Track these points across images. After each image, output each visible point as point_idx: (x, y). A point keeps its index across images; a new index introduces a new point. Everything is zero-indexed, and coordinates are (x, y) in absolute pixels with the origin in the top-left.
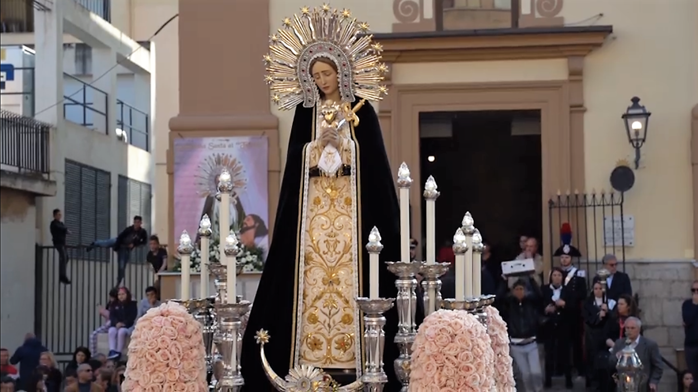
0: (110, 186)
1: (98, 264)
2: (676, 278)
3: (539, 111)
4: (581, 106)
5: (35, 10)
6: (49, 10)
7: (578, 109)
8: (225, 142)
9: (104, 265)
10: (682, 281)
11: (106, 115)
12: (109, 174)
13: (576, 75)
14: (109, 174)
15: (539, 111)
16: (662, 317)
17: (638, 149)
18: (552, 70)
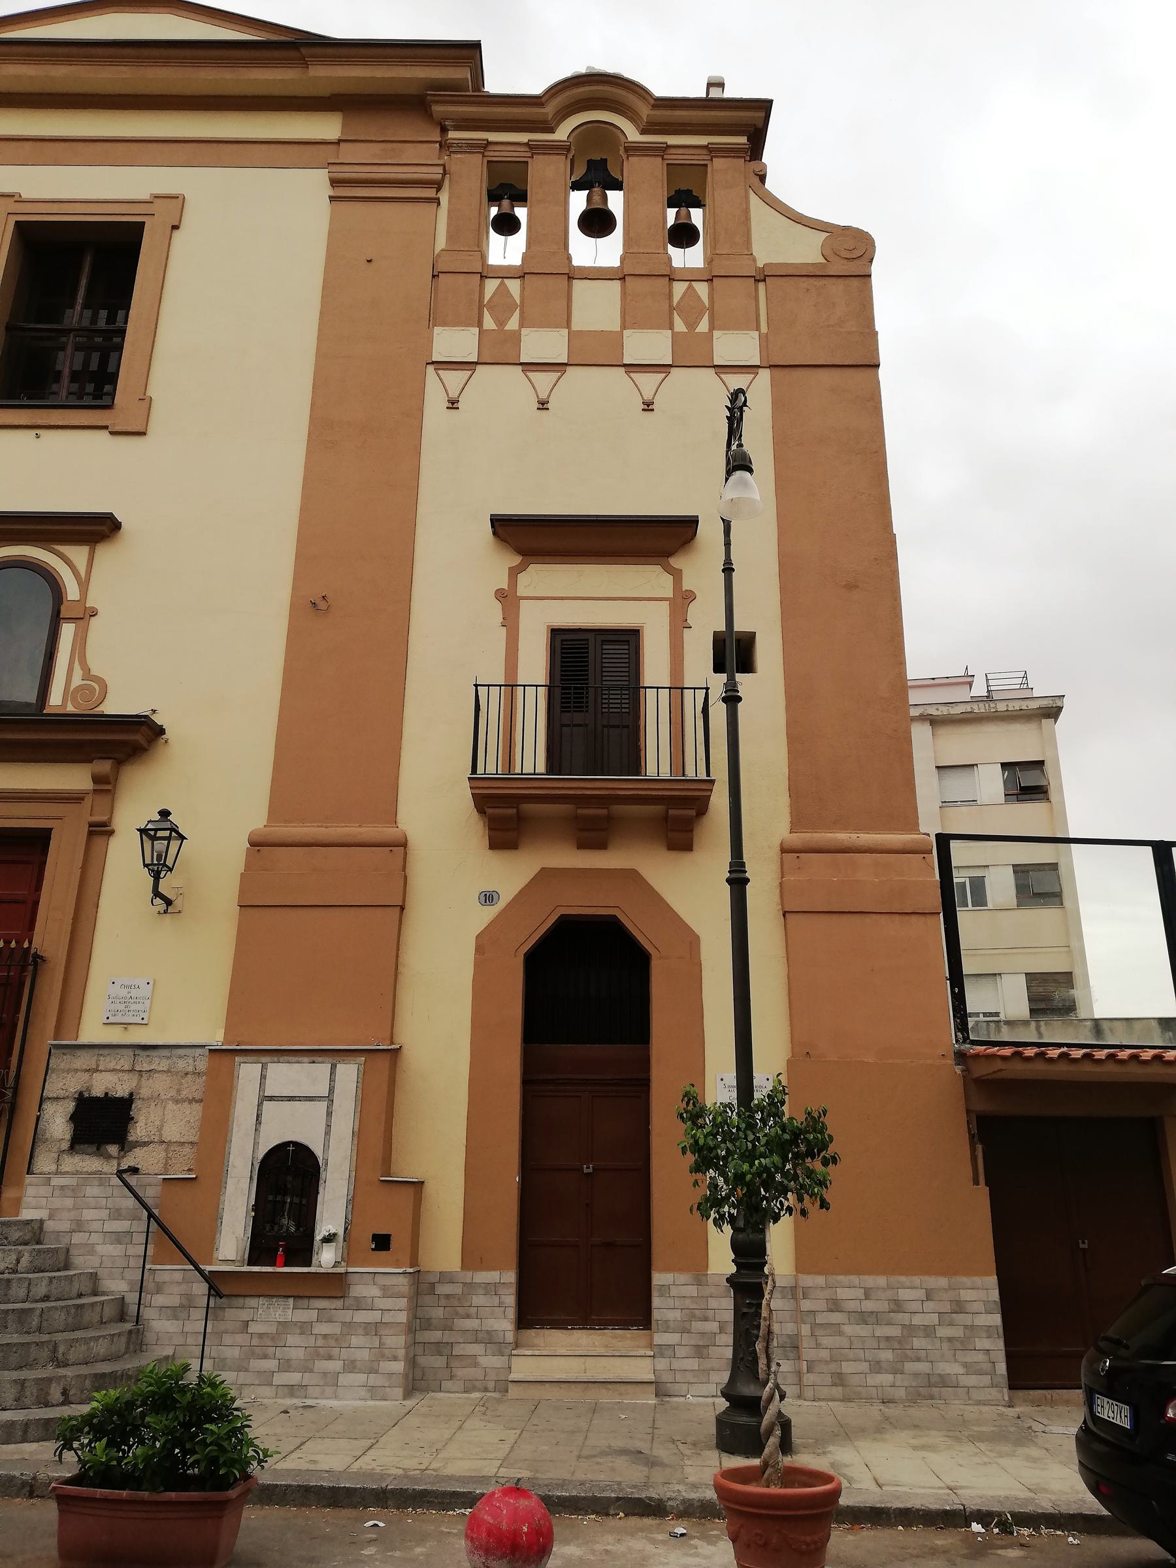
2: (190, 1069)
13: (106, 786)
18: (73, 778)
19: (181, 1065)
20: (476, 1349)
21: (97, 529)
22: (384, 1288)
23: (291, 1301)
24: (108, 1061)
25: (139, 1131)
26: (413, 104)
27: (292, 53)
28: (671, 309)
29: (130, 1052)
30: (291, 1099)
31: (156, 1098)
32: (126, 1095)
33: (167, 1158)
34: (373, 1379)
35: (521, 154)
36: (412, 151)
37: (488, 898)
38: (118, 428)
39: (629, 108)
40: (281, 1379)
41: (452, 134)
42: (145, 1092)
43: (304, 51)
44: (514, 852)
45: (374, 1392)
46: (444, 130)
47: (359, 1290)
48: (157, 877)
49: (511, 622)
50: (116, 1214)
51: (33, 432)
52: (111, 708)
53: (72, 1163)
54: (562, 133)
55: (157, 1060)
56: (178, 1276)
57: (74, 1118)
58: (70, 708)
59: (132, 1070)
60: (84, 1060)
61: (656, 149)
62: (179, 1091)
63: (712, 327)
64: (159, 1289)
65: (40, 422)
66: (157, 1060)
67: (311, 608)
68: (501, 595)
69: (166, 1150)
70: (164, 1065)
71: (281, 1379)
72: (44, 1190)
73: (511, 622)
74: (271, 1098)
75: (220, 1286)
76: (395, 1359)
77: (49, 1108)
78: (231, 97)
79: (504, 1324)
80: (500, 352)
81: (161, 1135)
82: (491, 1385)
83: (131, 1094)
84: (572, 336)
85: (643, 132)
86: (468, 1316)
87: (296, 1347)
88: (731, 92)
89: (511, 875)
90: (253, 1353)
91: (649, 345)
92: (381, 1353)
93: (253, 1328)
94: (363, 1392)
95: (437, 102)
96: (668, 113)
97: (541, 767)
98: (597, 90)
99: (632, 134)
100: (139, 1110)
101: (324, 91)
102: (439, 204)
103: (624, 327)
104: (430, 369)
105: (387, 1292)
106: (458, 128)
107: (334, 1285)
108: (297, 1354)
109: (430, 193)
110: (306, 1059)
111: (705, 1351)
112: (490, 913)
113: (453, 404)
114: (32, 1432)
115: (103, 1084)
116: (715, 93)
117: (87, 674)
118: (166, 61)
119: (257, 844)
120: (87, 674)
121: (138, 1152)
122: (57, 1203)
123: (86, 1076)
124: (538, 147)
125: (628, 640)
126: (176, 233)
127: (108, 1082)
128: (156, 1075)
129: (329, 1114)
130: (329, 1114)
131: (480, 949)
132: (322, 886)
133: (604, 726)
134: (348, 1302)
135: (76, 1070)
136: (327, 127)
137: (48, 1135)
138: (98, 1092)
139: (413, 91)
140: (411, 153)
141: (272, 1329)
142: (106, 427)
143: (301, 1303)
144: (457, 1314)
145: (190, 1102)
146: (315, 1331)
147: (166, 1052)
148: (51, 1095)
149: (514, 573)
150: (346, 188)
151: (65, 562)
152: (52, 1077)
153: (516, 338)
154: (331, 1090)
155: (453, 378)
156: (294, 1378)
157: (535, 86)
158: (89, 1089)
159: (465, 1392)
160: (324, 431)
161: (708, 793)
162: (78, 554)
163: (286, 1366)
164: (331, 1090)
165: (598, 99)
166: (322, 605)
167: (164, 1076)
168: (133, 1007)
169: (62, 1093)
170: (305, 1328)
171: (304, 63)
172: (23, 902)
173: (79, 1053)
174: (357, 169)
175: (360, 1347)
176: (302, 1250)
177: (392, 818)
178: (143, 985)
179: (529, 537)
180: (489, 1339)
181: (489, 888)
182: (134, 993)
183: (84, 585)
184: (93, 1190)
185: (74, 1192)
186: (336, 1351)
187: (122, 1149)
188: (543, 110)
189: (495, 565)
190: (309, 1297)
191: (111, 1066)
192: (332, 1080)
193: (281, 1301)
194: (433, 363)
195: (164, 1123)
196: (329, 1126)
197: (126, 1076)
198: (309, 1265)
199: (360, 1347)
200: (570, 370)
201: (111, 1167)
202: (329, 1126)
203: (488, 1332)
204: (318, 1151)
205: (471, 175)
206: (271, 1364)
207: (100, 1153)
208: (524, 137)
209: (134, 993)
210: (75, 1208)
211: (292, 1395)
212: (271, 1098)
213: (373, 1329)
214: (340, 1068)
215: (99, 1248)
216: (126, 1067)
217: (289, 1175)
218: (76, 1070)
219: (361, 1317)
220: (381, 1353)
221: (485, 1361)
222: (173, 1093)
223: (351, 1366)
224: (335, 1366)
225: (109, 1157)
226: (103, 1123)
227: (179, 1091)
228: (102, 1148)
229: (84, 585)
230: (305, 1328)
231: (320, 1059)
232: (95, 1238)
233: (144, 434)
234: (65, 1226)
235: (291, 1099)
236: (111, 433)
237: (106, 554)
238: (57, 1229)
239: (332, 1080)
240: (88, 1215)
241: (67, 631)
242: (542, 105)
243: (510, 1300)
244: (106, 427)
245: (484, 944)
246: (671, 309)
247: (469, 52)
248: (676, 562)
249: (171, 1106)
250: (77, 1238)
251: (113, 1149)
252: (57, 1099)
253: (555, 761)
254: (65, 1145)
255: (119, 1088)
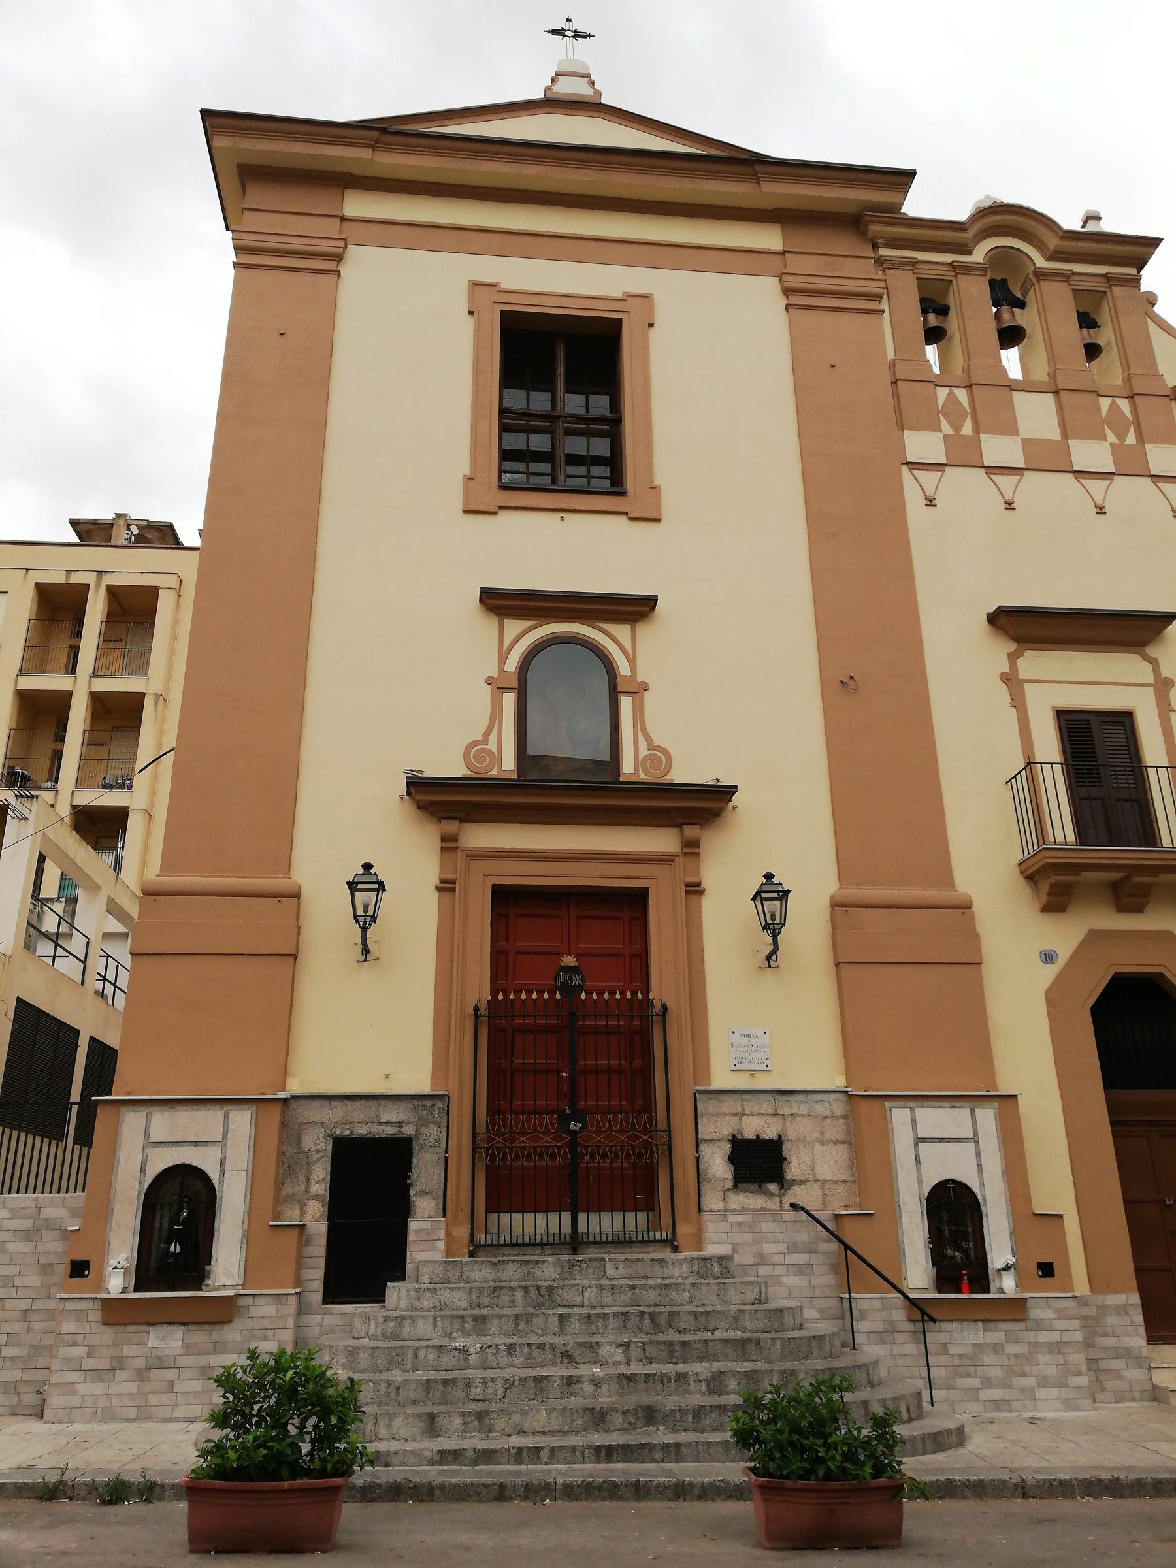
0: (77, 1046)
1: (46, 1141)
2: (828, 1113)
3: (645, 891)
4: (698, 885)
5: (9, 817)
6: (26, 819)
7: (695, 890)
8: (180, 1437)
9: (54, 1143)
10: (836, 1118)
11: (85, 963)
12: (78, 1032)
13: (692, 848)
14: (78, 1032)
15: (645, 891)
16: (813, 1168)
17: (775, 937)
18: (659, 841)
19: (819, 1109)
20: (1116, 1364)
21: (636, 609)
22: (1057, 1311)
23: (980, 1324)
24: (752, 1106)
25: (793, 1170)
26: (853, 222)
27: (748, 170)
28: (938, 412)
29: (769, 1097)
30: (941, 1140)
31: (801, 1140)
32: (775, 1137)
33: (824, 1195)
34: (1065, 1393)
35: (947, 274)
36: (848, 264)
37: (1048, 957)
38: (636, 515)
39: (1036, 238)
40: (986, 1394)
41: (883, 252)
42: (791, 1134)
43: (758, 168)
44: (1139, 915)
45: (1068, 1404)
46: (875, 247)
47: (1037, 1312)
48: (364, 929)
49: (1018, 702)
50: (794, 1248)
51: (559, 515)
52: (679, 776)
53: (739, 1200)
54: (979, 256)
55: (795, 1105)
56: (877, 1304)
57: (732, 1159)
58: (643, 777)
59: (775, 1114)
60: (729, 1105)
61: (908, 264)
62: (822, 1133)
63: (977, 431)
64: (863, 1317)
65: (563, 506)
66: (795, 1105)
67: (841, 687)
68: (1006, 678)
69: (822, 1188)
70: (803, 1109)
71: (986, 1394)
72: (722, 1227)
73: (1018, 702)
74: (924, 1140)
75: (922, 1313)
76: (1080, 1374)
77: (705, 1149)
78: (498, 189)
79: (1137, 1340)
80: (964, 456)
81: (814, 1174)
82: (1137, 1395)
83: (780, 1136)
84: (1026, 442)
85: (1049, 259)
86: (1106, 1335)
87: (992, 1365)
88: (1108, 225)
89: (1065, 935)
90: (957, 1373)
91: (1091, 454)
92: (1067, 1370)
93: (953, 1350)
94: (1059, 1405)
95: (873, 222)
96: (1073, 244)
97: (1071, 837)
98: (1004, 218)
99: (1040, 262)
100: (790, 1151)
101: (770, 205)
102: (339, 276)
103: (1065, 435)
104: (905, 469)
105: (1061, 1315)
106: (887, 246)
107: (1015, 1309)
108: (996, 1372)
109: (331, 265)
110: (947, 1104)
111: (146, 1374)
112: (1050, 973)
113: (930, 502)
114: (929, 1445)
115: (751, 1128)
116: (1092, 227)
117: (651, 746)
118: (628, 168)
119: (837, 905)
120: (651, 746)
121: (797, 1189)
122: (737, 1238)
123: (735, 1120)
124: (961, 268)
125: (1124, 720)
126: (652, 330)
127: (757, 1125)
128: (798, 1119)
129: (978, 1154)
130: (978, 1154)
131: (1050, 1002)
132: (896, 945)
133: (1117, 800)
134: (1030, 1324)
135: (724, 1114)
136: (769, 238)
137: (710, 1175)
138: (749, 1134)
139: (850, 209)
140: (851, 267)
141: (970, 1351)
142: (626, 513)
143: (992, 1325)
144: (1096, 1333)
145: (835, 1143)
146: (951, 1352)
147: (802, 1097)
148: (706, 1138)
149: (1013, 658)
150: (796, 296)
151: (612, 638)
152: (702, 1121)
153: (975, 444)
154: (975, 1132)
155: (928, 478)
156: (997, 1394)
157: (961, 214)
158: (740, 1131)
159: (1116, 1402)
160: (822, 525)
161: (685, 850)
162: (621, 631)
163: (987, 1383)
164: (975, 1132)
165: (1008, 227)
166: (851, 684)
167: (805, 1120)
168: (756, 1055)
169: (716, 1136)
170: (997, 1348)
171: (756, 179)
172: (619, 955)
173: (723, 1097)
174: (252, 237)
175: (1048, 1364)
176: (980, 1278)
177: (285, 865)
178: (760, 1034)
179: (1026, 627)
180: (1127, 1354)
181: (1048, 948)
182: (754, 1041)
183: (632, 661)
184: (767, 1226)
185: (751, 1227)
186: (1028, 1369)
187: (782, 1187)
188: (966, 235)
189: (995, 652)
190: (995, 1321)
191: (756, 1109)
192: (974, 1124)
193: (972, 1325)
194: (907, 463)
195: (816, 1161)
196: (980, 1165)
197: (771, 1120)
198: (988, 1291)
199: (1048, 1364)
200: (1027, 475)
201: (773, 1204)
202: (980, 1165)
203: (1126, 1348)
204: (975, 1187)
205: (905, 291)
206: (974, 1382)
207: (761, 1191)
208: (947, 258)
209: (754, 1041)
210: (755, 1242)
211: (998, 1410)
212: (924, 1140)
213: (1056, 1348)
214: (979, 1112)
215: (785, 1279)
216: (770, 1111)
217: (953, 1210)
218: (724, 1114)
219: (1043, 1337)
220: (1067, 1370)
221: (1128, 1374)
222: (817, 1135)
223: (1043, 1382)
224: (1030, 1382)
225: (770, 1195)
226: (759, 1163)
227: (822, 1133)
228: (763, 1186)
229: (632, 661)
230: (997, 1348)
231: (959, 1104)
232: (779, 1270)
233: (659, 520)
234: (750, 1260)
235: (941, 1140)
236: (630, 519)
237: (644, 630)
238: (743, 1262)
239: (974, 1124)
240: (768, 1248)
241: (626, 703)
242: (965, 230)
243: (1139, 1319)
244: (626, 513)
245: (1054, 998)
246: (938, 412)
247: (903, 178)
248: (1151, 651)
249: (817, 1147)
250: (764, 1271)
251: (773, 1187)
252: (712, 1141)
253: (1082, 835)
254: (729, 1184)
255: (768, 1131)
